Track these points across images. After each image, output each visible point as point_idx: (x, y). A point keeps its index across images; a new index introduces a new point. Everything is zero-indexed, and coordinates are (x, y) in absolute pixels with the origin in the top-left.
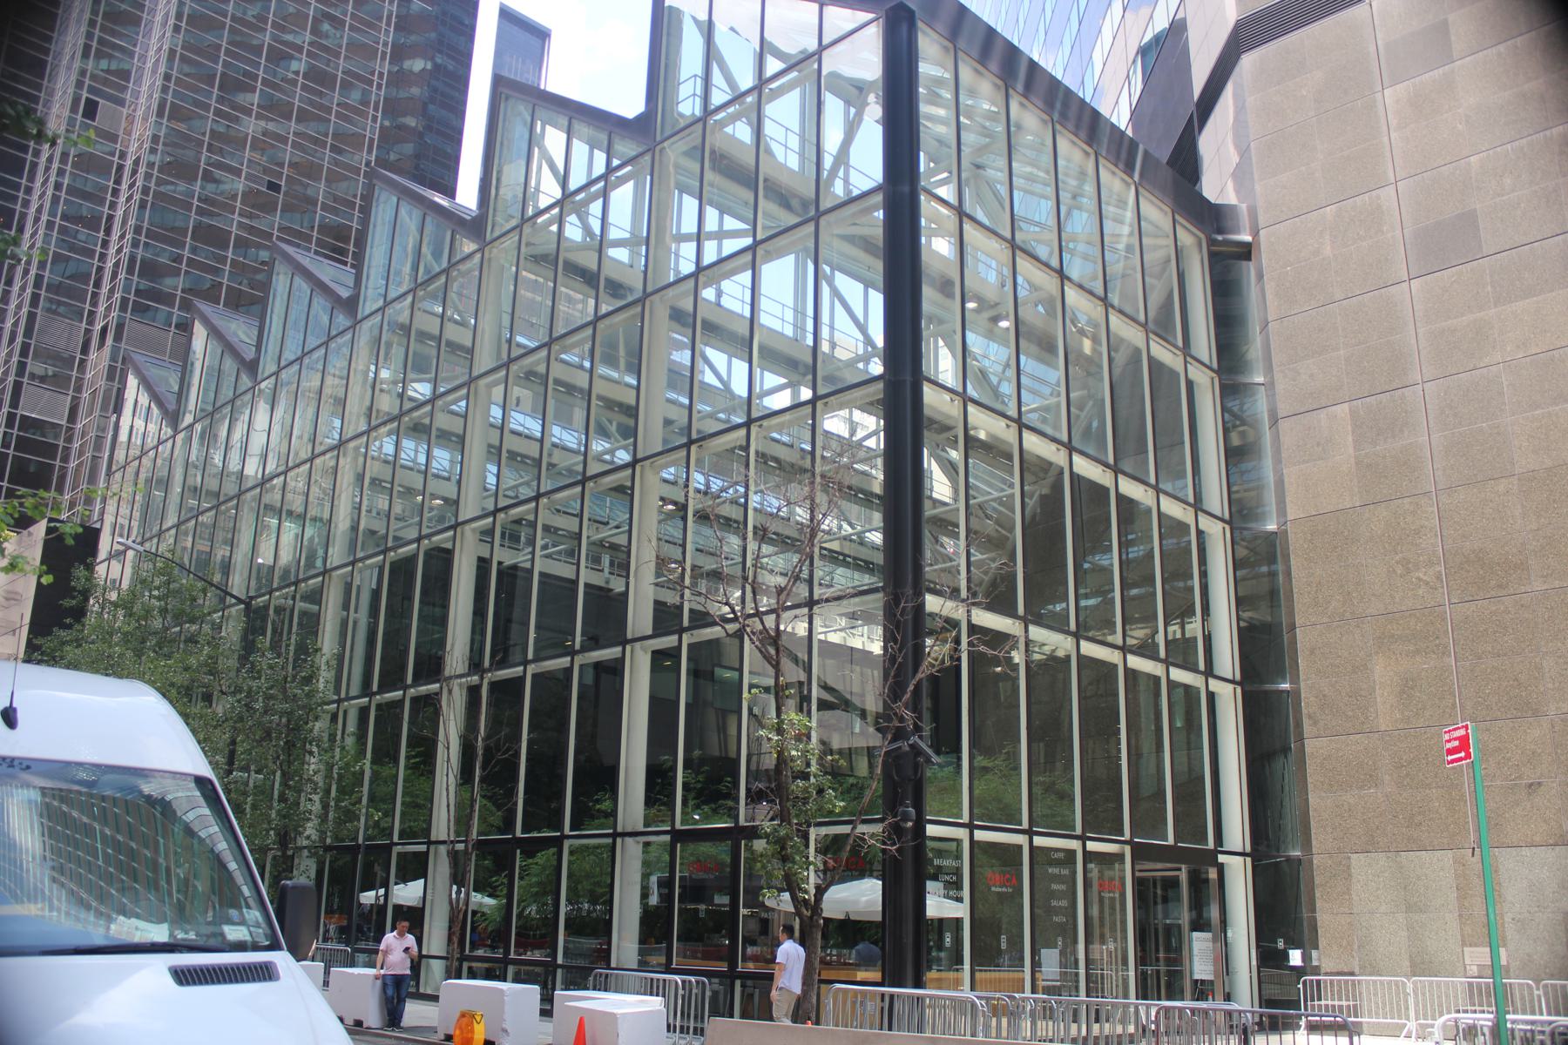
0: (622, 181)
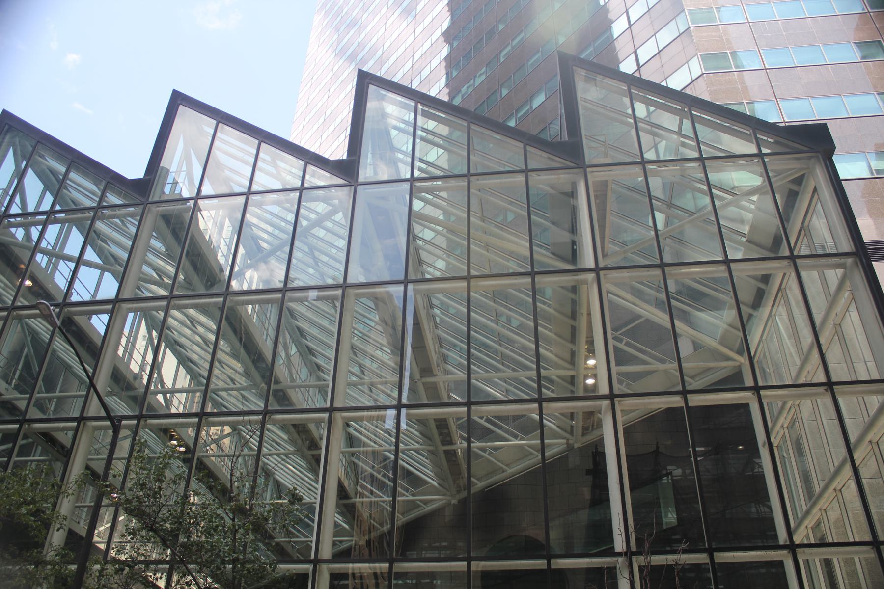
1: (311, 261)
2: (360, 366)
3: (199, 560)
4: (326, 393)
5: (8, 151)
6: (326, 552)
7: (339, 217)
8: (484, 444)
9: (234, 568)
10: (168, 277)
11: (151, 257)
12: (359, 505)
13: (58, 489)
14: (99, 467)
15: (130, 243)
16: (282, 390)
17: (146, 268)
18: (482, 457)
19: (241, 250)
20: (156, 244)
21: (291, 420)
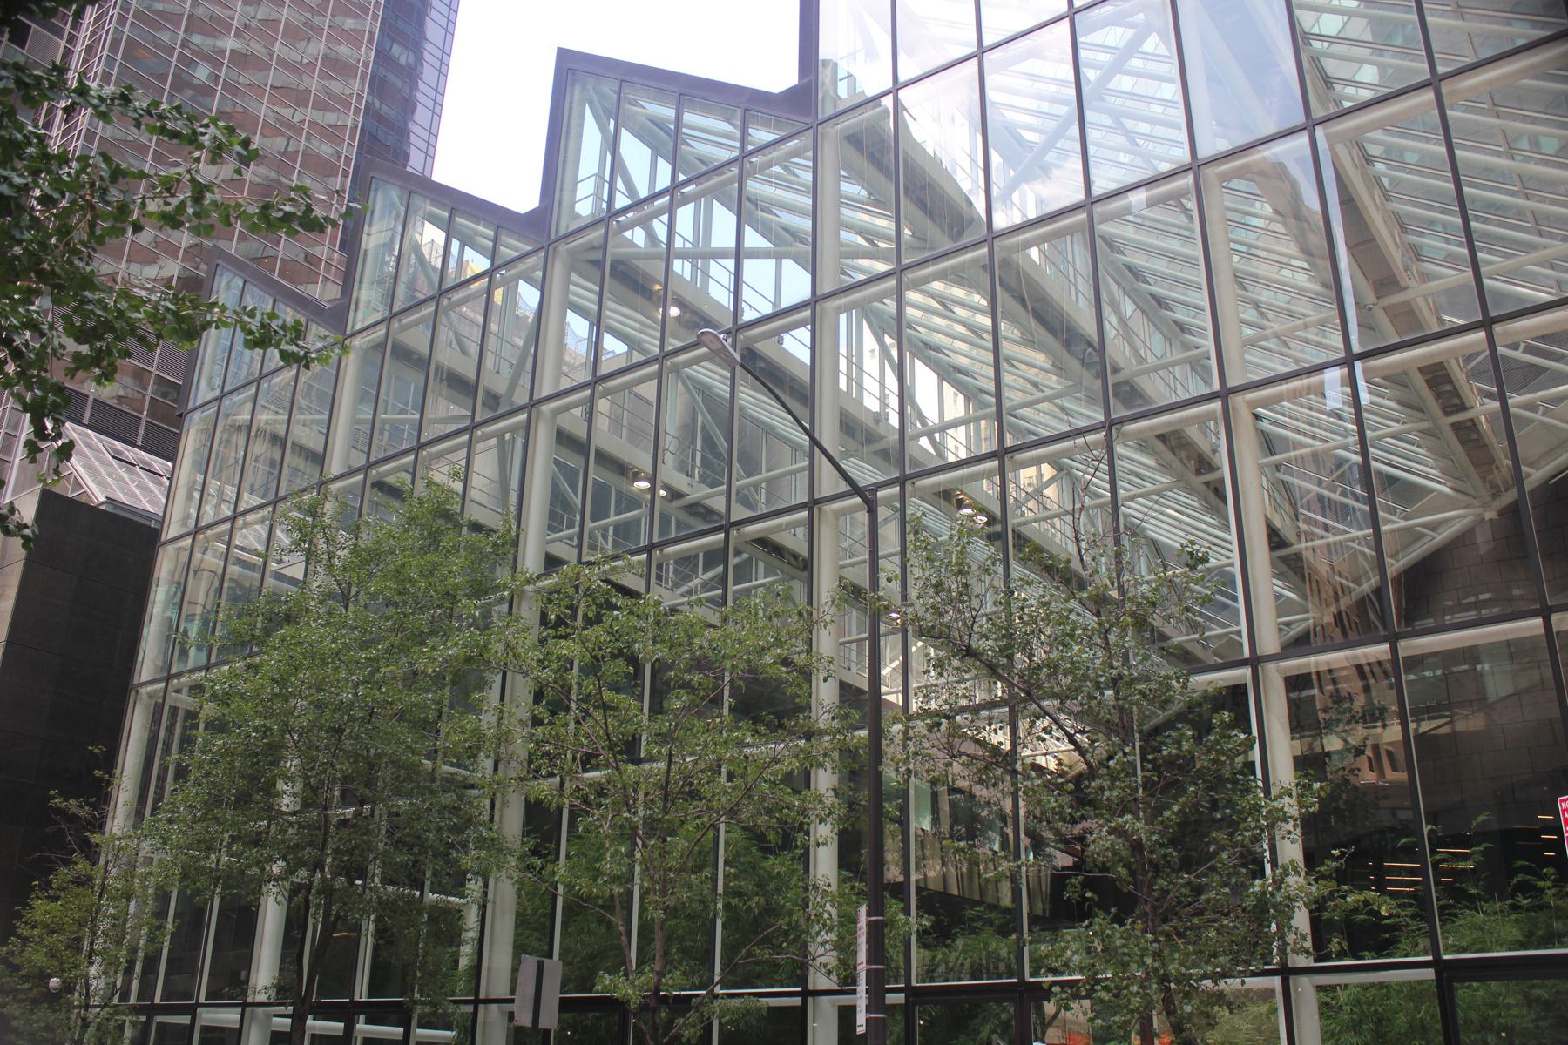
0: (686, 200)
1: (1121, 140)
2: (1257, 305)
3: (1056, 690)
4: (1208, 370)
5: (582, 115)
6: (1269, 642)
7: (1152, 44)
8: (1530, 396)
9: (1117, 693)
10: (886, 238)
11: (848, 214)
12: (1307, 555)
13: (809, 622)
14: (861, 577)
15: (809, 201)
16: (1126, 382)
17: (846, 236)
18: (1533, 421)
19: (995, 159)
20: (851, 189)
21: (1151, 428)
